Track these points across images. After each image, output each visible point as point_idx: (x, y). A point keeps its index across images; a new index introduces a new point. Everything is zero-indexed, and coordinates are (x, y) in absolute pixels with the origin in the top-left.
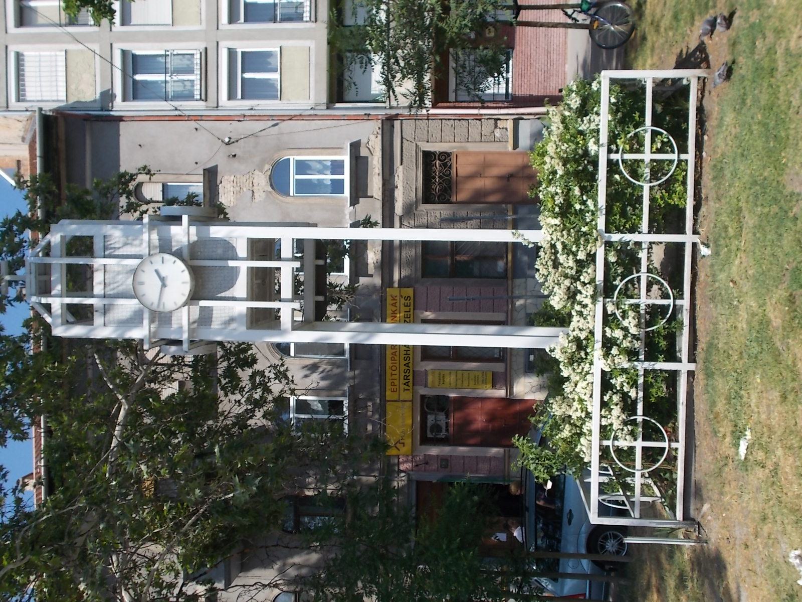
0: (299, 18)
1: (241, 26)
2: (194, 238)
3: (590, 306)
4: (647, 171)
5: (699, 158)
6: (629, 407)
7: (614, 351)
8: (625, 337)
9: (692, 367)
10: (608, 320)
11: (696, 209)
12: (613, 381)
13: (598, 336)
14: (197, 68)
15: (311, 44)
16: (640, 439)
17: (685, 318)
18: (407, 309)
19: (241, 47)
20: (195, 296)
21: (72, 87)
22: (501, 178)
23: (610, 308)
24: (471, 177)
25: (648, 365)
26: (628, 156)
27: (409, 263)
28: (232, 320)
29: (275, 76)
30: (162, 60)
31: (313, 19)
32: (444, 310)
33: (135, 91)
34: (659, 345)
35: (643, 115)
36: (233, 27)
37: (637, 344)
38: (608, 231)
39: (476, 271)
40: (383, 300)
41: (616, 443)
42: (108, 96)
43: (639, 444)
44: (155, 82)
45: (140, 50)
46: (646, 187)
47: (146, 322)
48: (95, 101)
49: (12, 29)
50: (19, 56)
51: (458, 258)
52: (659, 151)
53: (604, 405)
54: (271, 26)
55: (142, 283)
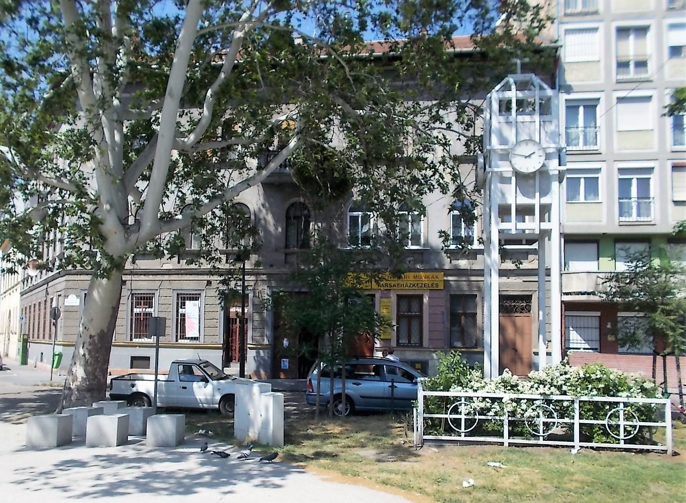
0: (621, 214)
1: (616, 176)
2: (551, 173)
3: (538, 392)
4: (614, 423)
5: (620, 450)
6: (483, 411)
7: (514, 404)
8: (523, 410)
9: (506, 444)
10: (531, 401)
11: (592, 448)
12: (496, 403)
13: (521, 396)
14: (588, 148)
15: (604, 221)
16: (466, 417)
17: (532, 442)
18: (430, 285)
19: (602, 177)
20: (518, 174)
21: (575, 66)
22: (514, 344)
23: (537, 403)
24: (514, 324)
25: (506, 422)
26: (621, 413)
27: (459, 287)
28: (503, 194)
29: (582, 199)
30: (592, 125)
31: (621, 223)
32: (430, 309)
33: (572, 107)
34: (516, 428)
35: (643, 421)
36: (616, 171)
37: (519, 416)
38: (580, 402)
39: (455, 329)
40: (436, 270)
41: (463, 405)
42: (568, 89)
43: (463, 417)
44: (577, 120)
45: (600, 110)
46: (605, 422)
47: (503, 147)
48: (565, 81)
49: (615, 25)
50: (595, 30)
51: (463, 317)
52: (625, 429)
53: (484, 399)
54: (616, 196)
55: (527, 144)
